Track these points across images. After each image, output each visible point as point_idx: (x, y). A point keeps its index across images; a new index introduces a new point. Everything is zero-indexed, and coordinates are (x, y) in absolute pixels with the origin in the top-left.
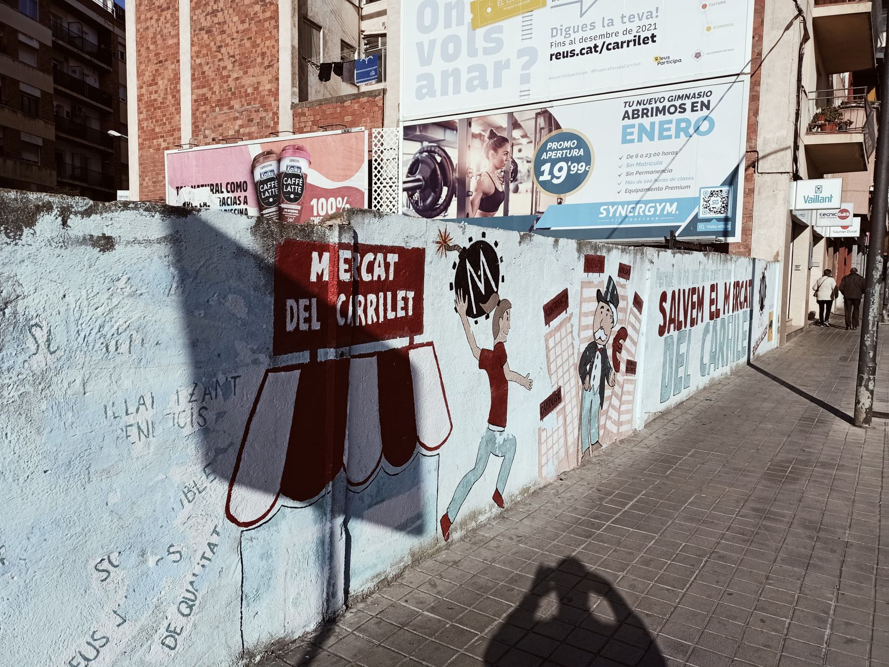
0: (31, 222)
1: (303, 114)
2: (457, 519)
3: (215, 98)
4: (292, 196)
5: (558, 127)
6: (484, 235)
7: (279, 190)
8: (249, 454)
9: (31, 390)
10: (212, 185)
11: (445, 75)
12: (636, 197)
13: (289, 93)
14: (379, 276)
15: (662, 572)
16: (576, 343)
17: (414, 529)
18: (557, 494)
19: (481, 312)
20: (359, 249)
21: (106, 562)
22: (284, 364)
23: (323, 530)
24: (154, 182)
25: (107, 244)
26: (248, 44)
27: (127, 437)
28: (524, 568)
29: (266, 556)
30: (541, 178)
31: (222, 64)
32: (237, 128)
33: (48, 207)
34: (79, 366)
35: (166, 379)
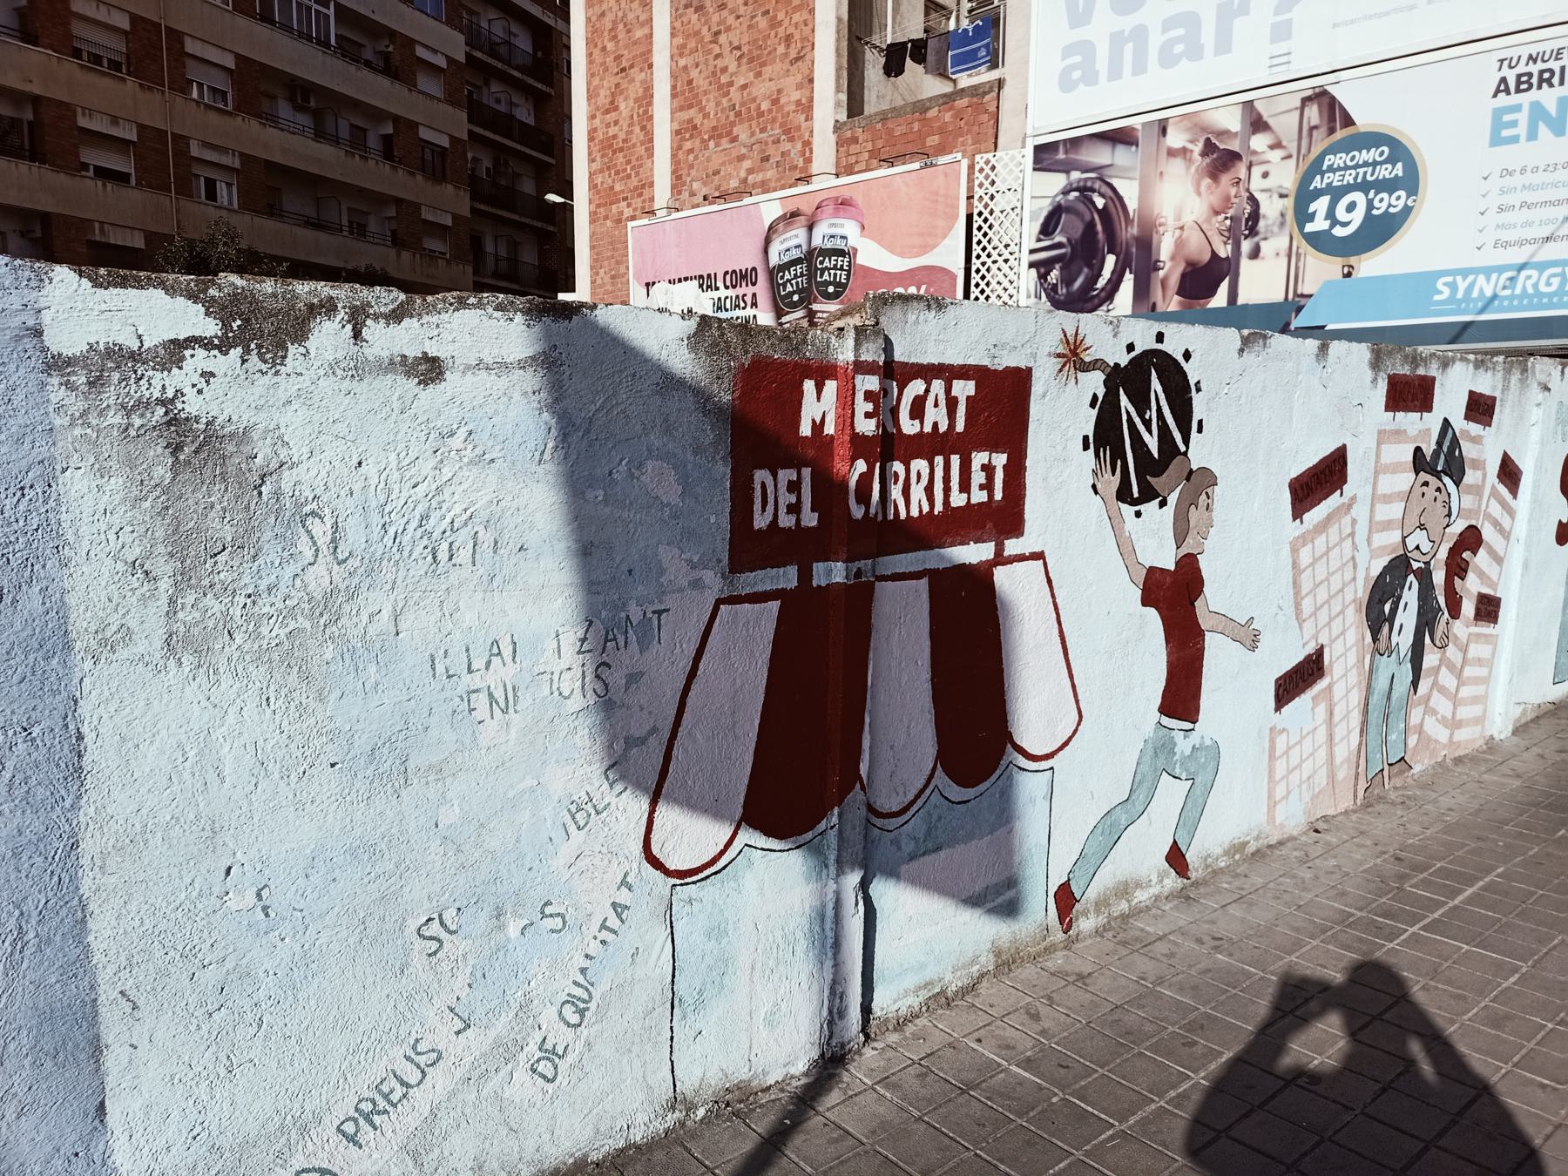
0: (300, 334)
1: (855, 140)
2: (1089, 893)
3: (708, 124)
4: (831, 289)
5: (1348, 121)
6: (1160, 337)
7: (809, 281)
8: (686, 750)
9: (307, 625)
10: (701, 277)
11: (1117, 40)
12: (1517, 256)
13: (831, 104)
14: (935, 425)
15: (1532, 1045)
16: (1363, 557)
17: (1001, 905)
18: (1305, 860)
19: (1149, 494)
20: (894, 372)
21: (436, 924)
22: (748, 590)
23: (822, 894)
24: (613, 277)
25: (431, 371)
26: (762, 23)
27: (471, 710)
28: (1223, 1003)
29: (717, 932)
30: (1309, 228)
31: (720, 63)
32: (743, 174)
33: (329, 307)
34: (388, 586)
35: (540, 609)
